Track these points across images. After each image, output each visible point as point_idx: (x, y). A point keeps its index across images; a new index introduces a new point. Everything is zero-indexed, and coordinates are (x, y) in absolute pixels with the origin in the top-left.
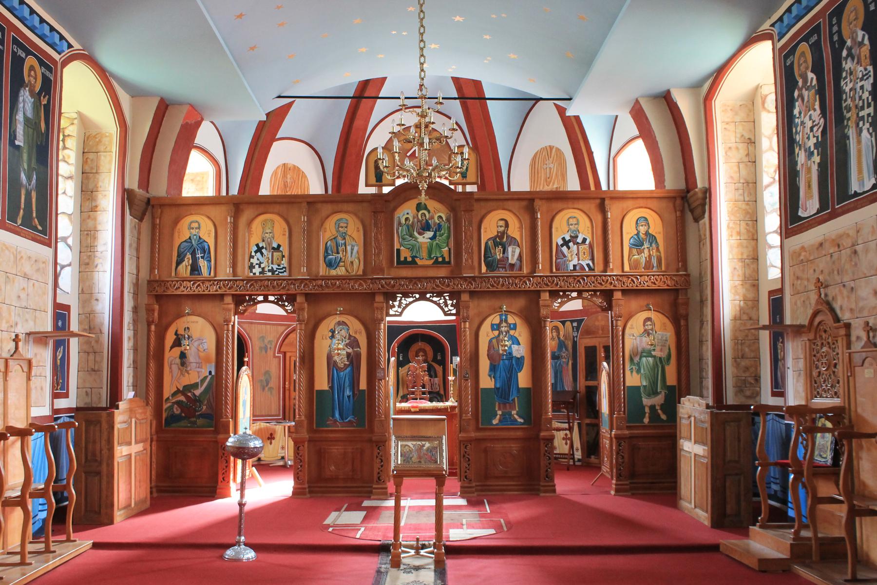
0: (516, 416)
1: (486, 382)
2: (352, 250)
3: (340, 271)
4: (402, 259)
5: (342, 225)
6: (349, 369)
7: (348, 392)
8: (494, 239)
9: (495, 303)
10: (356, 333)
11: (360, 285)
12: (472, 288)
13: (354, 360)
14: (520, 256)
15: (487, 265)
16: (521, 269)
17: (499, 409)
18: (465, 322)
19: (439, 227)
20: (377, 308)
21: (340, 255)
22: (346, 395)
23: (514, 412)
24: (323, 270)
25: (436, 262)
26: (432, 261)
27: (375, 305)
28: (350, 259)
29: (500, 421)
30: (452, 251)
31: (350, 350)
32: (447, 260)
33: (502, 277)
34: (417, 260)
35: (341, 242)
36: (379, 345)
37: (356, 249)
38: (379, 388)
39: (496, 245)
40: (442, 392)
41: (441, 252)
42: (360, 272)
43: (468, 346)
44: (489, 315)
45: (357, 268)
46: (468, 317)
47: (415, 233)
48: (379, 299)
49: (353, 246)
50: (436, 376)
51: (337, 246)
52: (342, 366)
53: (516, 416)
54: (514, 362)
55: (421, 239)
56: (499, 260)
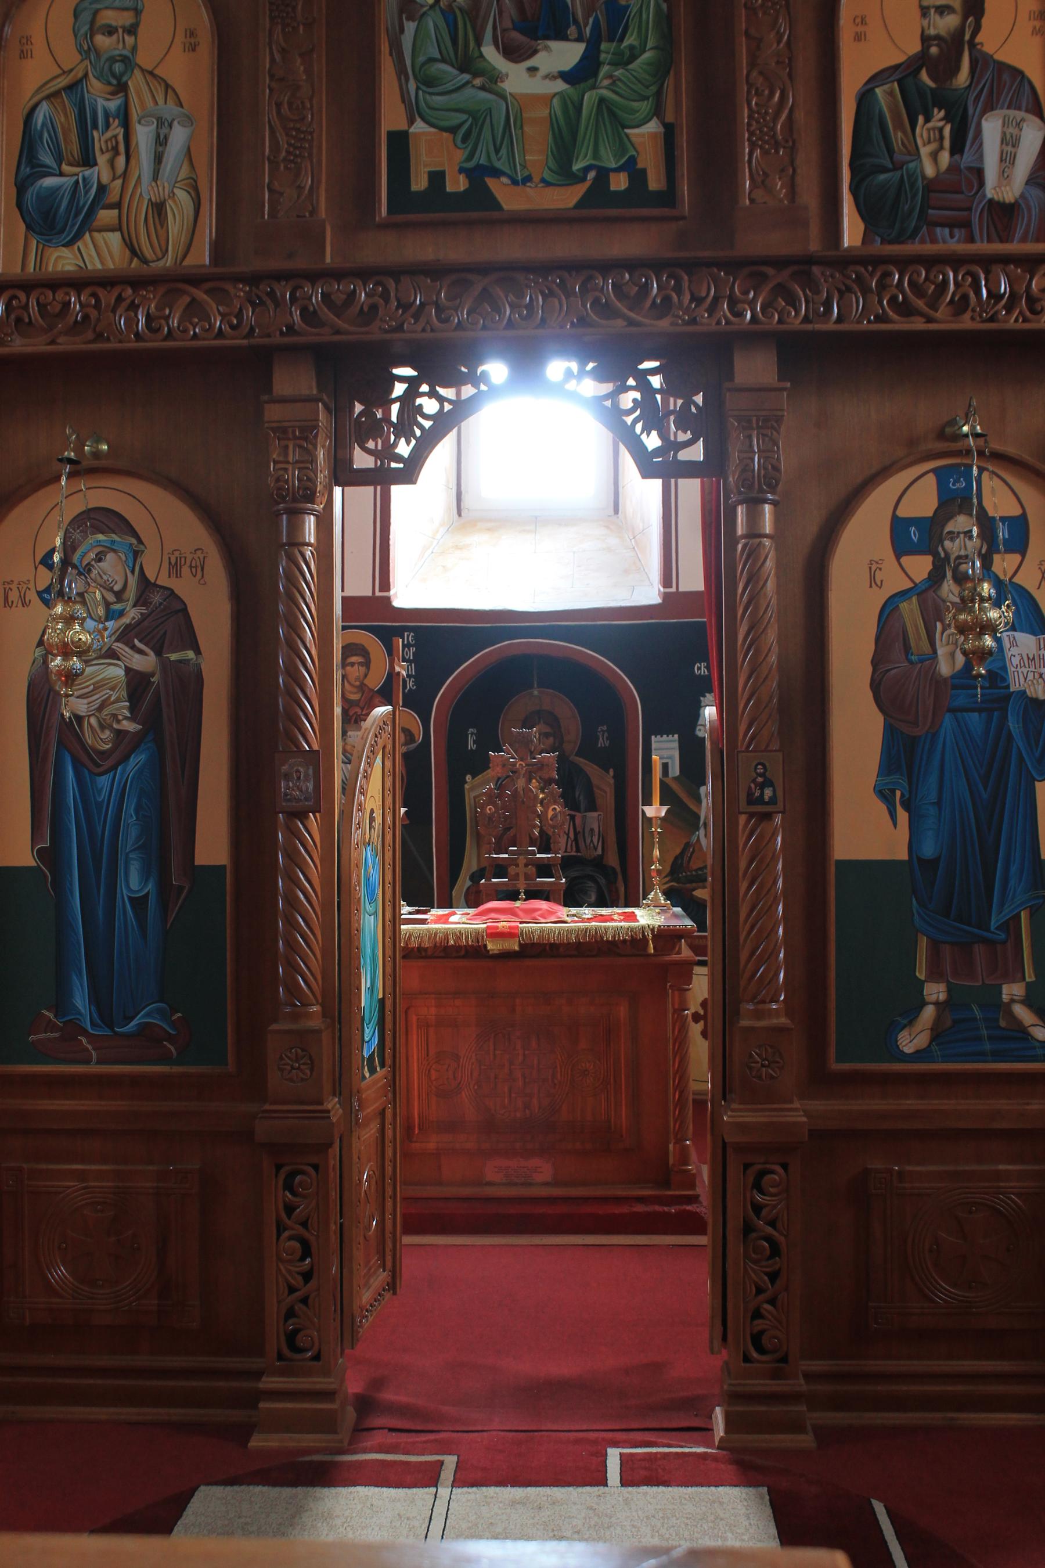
0: (1020, 1011)
1: (867, 829)
2: (161, 141)
3: (101, 251)
4: (419, 183)
5: (109, 17)
6: (138, 760)
7: (134, 881)
8: (904, 74)
9: (921, 410)
10: (175, 569)
11: (194, 309)
12: (795, 321)
13: (164, 709)
15: (866, 211)
17: (935, 974)
18: (754, 503)
20: (282, 432)
21: (101, 171)
22: (123, 893)
23: (1011, 991)
25: (599, 193)
26: (578, 192)
27: (273, 413)
28: (147, 191)
29: (937, 1034)
30: (683, 140)
31: (145, 661)
32: (655, 182)
33: (956, 261)
34: (498, 187)
36: (295, 629)
37: (179, 136)
38: (293, 857)
39: (917, 104)
40: (613, 860)
41: (622, 144)
42: (202, 256)
43: (772, 636)
44: (884, 472)
45: (186, 235)
46: (771, 479)
47: (491, 53)
48: (294, 381)
49: (163, 124)
50: (592, 807)
51: (85, 124)
52: (104, 741)
53: (1020, 1011)
54: (1014, 725)
55: (516, 80)
56: (931, 186)
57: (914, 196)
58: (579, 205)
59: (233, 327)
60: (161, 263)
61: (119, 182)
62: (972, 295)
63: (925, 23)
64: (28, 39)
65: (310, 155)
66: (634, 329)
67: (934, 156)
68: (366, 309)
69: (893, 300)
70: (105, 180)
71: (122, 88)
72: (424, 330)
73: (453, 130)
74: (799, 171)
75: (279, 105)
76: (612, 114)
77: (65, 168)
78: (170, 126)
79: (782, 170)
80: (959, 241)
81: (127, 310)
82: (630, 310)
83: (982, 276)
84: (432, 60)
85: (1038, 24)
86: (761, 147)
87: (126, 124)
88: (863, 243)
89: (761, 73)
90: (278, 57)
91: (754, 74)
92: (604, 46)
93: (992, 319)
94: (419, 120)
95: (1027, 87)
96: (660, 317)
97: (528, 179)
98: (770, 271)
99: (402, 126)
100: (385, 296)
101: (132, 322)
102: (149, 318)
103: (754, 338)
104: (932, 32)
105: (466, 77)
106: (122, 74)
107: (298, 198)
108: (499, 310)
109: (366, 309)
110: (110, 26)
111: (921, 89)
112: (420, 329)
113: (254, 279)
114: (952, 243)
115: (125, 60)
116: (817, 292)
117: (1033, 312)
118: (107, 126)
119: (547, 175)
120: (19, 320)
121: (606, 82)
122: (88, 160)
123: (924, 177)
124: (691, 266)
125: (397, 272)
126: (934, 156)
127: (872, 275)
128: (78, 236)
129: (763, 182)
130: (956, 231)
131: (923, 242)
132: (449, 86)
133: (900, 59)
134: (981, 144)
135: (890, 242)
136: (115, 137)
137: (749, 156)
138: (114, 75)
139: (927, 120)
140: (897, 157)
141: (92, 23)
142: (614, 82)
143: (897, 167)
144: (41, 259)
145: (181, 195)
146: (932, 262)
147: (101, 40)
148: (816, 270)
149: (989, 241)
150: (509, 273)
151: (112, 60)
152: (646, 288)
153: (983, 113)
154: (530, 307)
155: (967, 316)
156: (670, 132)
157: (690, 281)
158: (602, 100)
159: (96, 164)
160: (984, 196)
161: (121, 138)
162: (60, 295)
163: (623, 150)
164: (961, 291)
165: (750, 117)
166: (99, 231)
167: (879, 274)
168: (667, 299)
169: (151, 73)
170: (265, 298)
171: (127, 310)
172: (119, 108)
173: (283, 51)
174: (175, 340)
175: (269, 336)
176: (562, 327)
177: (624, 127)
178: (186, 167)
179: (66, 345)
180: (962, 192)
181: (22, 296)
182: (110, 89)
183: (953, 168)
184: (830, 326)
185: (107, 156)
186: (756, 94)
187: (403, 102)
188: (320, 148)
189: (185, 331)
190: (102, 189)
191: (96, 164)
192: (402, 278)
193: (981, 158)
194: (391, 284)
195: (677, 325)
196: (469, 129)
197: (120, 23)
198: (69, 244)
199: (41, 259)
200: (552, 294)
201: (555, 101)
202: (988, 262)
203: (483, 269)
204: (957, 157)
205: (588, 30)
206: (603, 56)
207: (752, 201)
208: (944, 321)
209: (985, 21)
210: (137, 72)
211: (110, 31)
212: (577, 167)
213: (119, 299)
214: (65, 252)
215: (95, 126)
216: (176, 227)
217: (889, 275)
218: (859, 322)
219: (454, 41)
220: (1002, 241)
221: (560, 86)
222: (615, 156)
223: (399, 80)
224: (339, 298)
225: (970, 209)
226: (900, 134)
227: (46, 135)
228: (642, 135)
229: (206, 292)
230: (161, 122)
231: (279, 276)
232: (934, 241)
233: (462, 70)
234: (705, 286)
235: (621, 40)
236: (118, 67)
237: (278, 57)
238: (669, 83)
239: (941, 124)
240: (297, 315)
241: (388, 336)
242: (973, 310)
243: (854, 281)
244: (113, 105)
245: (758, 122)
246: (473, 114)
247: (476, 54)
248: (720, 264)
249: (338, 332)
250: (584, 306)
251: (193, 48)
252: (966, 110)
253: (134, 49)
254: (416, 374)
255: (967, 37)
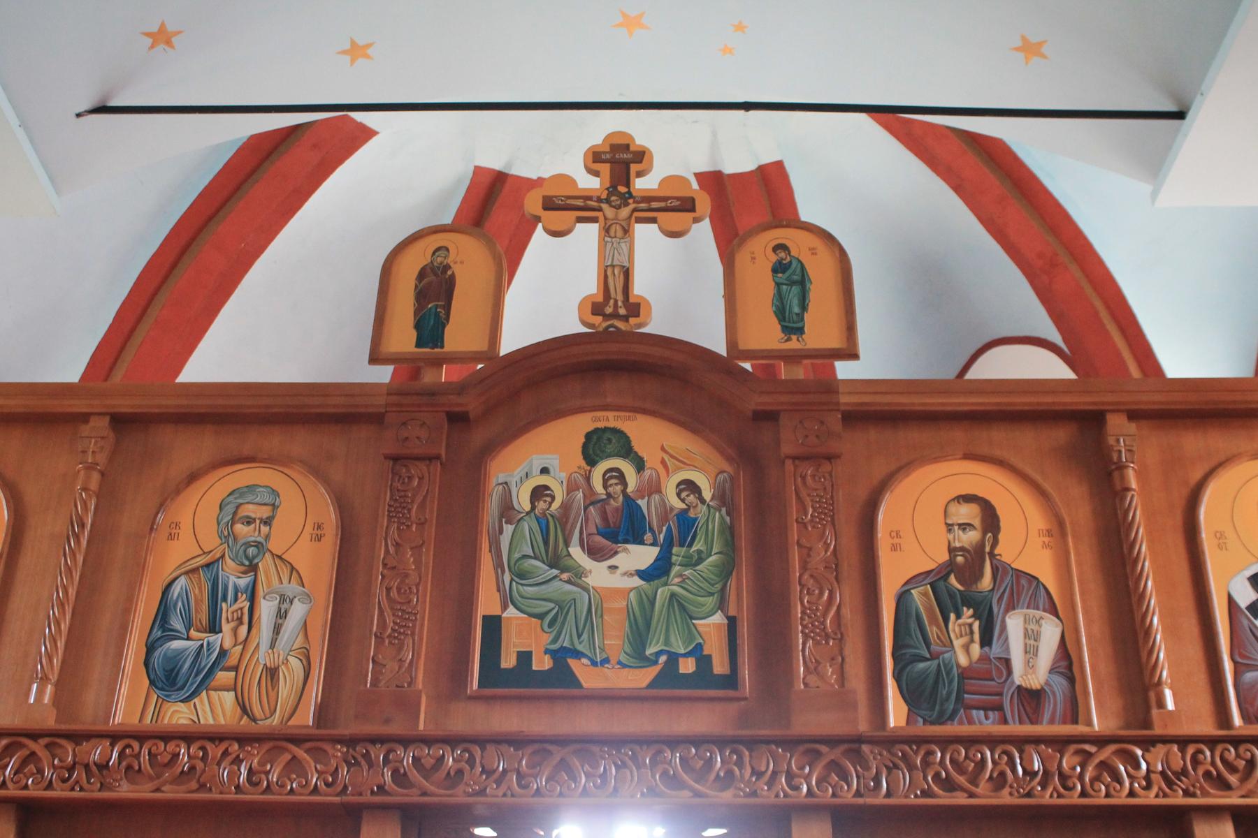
2: (282, 615)
3: (215, 709)
4: (508, 661)
5: (249, 510)
8: (936, 579)
11: (294, 765)
12: (847, 796)
14: (1066, 660)
15: (910, 694)
16: (1074, 712)
19: (685, 527)
21: (224, 638)
24: (129, 701)
25: (669, 676)
26: (653, 671)
28: (264, 656)
30: (744, 630)
32: (720, 667)
33: (992, 741)
35: (233, 578)
37: (298, 611)
39: (947, 604)
41: (690, 634)
42: (306, 717)
45: (295, 699)
51: (216, 596)
55: (598, 575)
56: (965, 674)
57: (951, 682)
58: (652, 685)
59: (328, 785)
60: (268, 722)
61: (240, 648)
62: (1009, 772)
63: (951, 537)
64: (177, 525)
65: (413, 634)
66: (698, 800)
67: (966, 648)
68: (452, 773)
69: (937, 776)
70: (227, 645)
71: (253, 568)
72: (505, 795)
73: (541, 617)
74: (847, 660)
75: (388, 589)
76: (683, 608)
77: (193, 633)
78: (291, 602)
79: (833, 659)
80: (993, 723)
81: (232, 763)
82: (696, 782)
83: (1017, 755)
84: (525, 557)
85: (1046, 539)
86: (813, 639)
87: (252, 599)
88: (908, 723)
89: (812, 576)
90: (392, 550)
91: (806, 576)
92: (675, 550)
93: (1029, 795)
94: (511, 607)
95: (1042, 589)
96: (723, 789)
97: (606, 661)
98: (824, 749)
99: (496, 611)
100: (471, 762)
101: (234, 775)
102: (251, 771)
103: (809, 810)
104: (958, 545)
105: (555, 572)
106: (254, 557)
107: (400, 668)
108: (574, 778)
109: (452, 773)
110: (248, 517)
111: (951, 594)
112: (501, 794)
113: (351, 742)
114: (986, 724)
115: (258, 545)
116: (868, 768)
117: (1066, 788)
118: (236, 599)
119: (623, 658)
120: (129, 767)
121: (677, 580)
122: (214, 628)
123: (958, 666)
124: (753, 743)
125: (482, 741)
126: (966, 648)
127: (916, 753)
128: (195, 693)
129: (816, 669)
130: (990, 713)
131: (961, 723)
132: (540, 579)
133: (932, 566)
134: (1007, 639)
135: (932, 723)
136: (241, 609)
137: (802, 646)
138: (247, 557)
139: (958, 617)
140: (934, 648)
141: (235, 513)
142: (683, 581)
143: (934, 656)
144: (158, 712)
145: (295, 663)
146: (971, 742)
147: (239, 527)
148: (865, 748)
149: (1021, 722)
150: (584, 744)
151: (248, 545)
152: (709, 763)
153: (1007, 611)
154: (604, 777)
155: (1006, 790)
156: (732, 622)
157: (751, 756)
158: (673, 595)
159: (221, 631)
160: (1013, 682)
161: (246, 610)
162: (171, 747)
163: (691, 637)
164: (999, 768)
165: (803, 613)
166: (215, 690)
167: (922, 752)
168: (730, 773)
169: (280, 557)
170: (360, 759)
171: (232, 763)
172: (248, 586)
173: (397, 545)
174: (273, 794)
175: (361, 794)
176: (632, 797)
177: (692, 618)
178: (301, 637)
179: (171, 793)
180: (993, 680)
181: (136, 745)
182: (243, 568)
183: (984, 658)
184: (880, 800)
185: (232, 624)
186: (808, 593)
187: (499, 591)
188: (422, 625)
189: (283, 786)
190: (223, 653)
191: (221, 631)
192: (488, 746)
193: (1007, 650)
194: (477, 751)
195: (740, 796)
196: (555, 616)
197: (259, 515)
198: (185, 701)
199: (158, 712)
200: (624, 765)
201: (632, 594)
202: (1021, 742)
203: (562, 741)
204: (986, 649)
205: (662, 536)
206: (674, 558)
207: (806, 685)
208: (985, 796)
209: (1001, 537)
210: (268, 556)
211: (249, 521)
212: (649, 651)
213: (226, 753)
214: (182, 707)
215: (225, 599)
216: (286, 690)
217: (930, 753)
218: (907, 797)
219: (546, 542)
220: (1032, 723)
221: (637, 582)
222: (684, 643)
223: (497, 573)
224: (428, 762)
225: (1000, 694)
226: (935, 629)
227: (180, 604)
228: (709, 625)
229: (307, 751)
230: (283, 598)
231: (374, 740)
232: (971, 722)
233: (551, 567)
234: (764, 763)
235: (690, 545)
236: (252, 551)
237: (392, 550)
238: (732, 583)
239: (970, 620)
240: (388, 775)
241: (471, 800)
242: (1011, 787)
243: (900, 759)
244: (243, 582)
245: (810, 617)
246: (560, 604)
247: (565, 553)
248: (779, 742)
249: (424, 794)
250: (653, 776)
251: (319, 538)
252: (991, 608)
253: (267, 537)
254: (495, 834)
255: (988, 549)
